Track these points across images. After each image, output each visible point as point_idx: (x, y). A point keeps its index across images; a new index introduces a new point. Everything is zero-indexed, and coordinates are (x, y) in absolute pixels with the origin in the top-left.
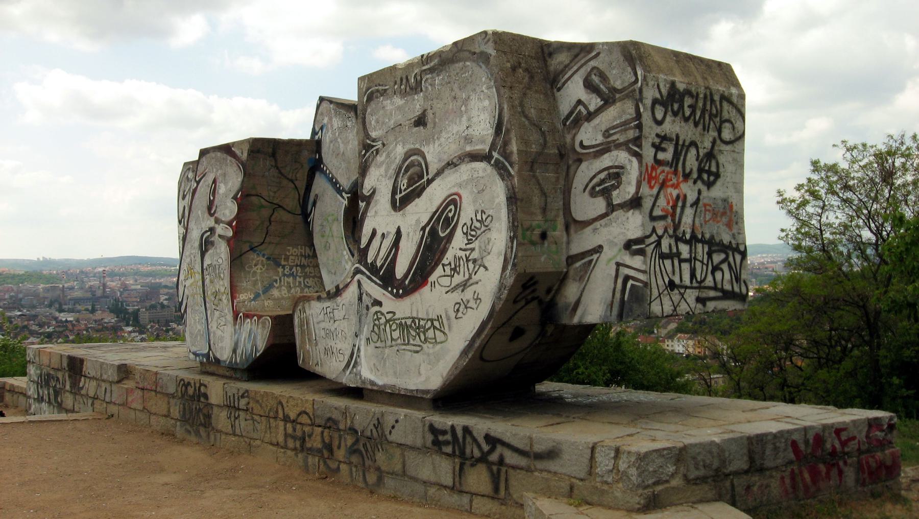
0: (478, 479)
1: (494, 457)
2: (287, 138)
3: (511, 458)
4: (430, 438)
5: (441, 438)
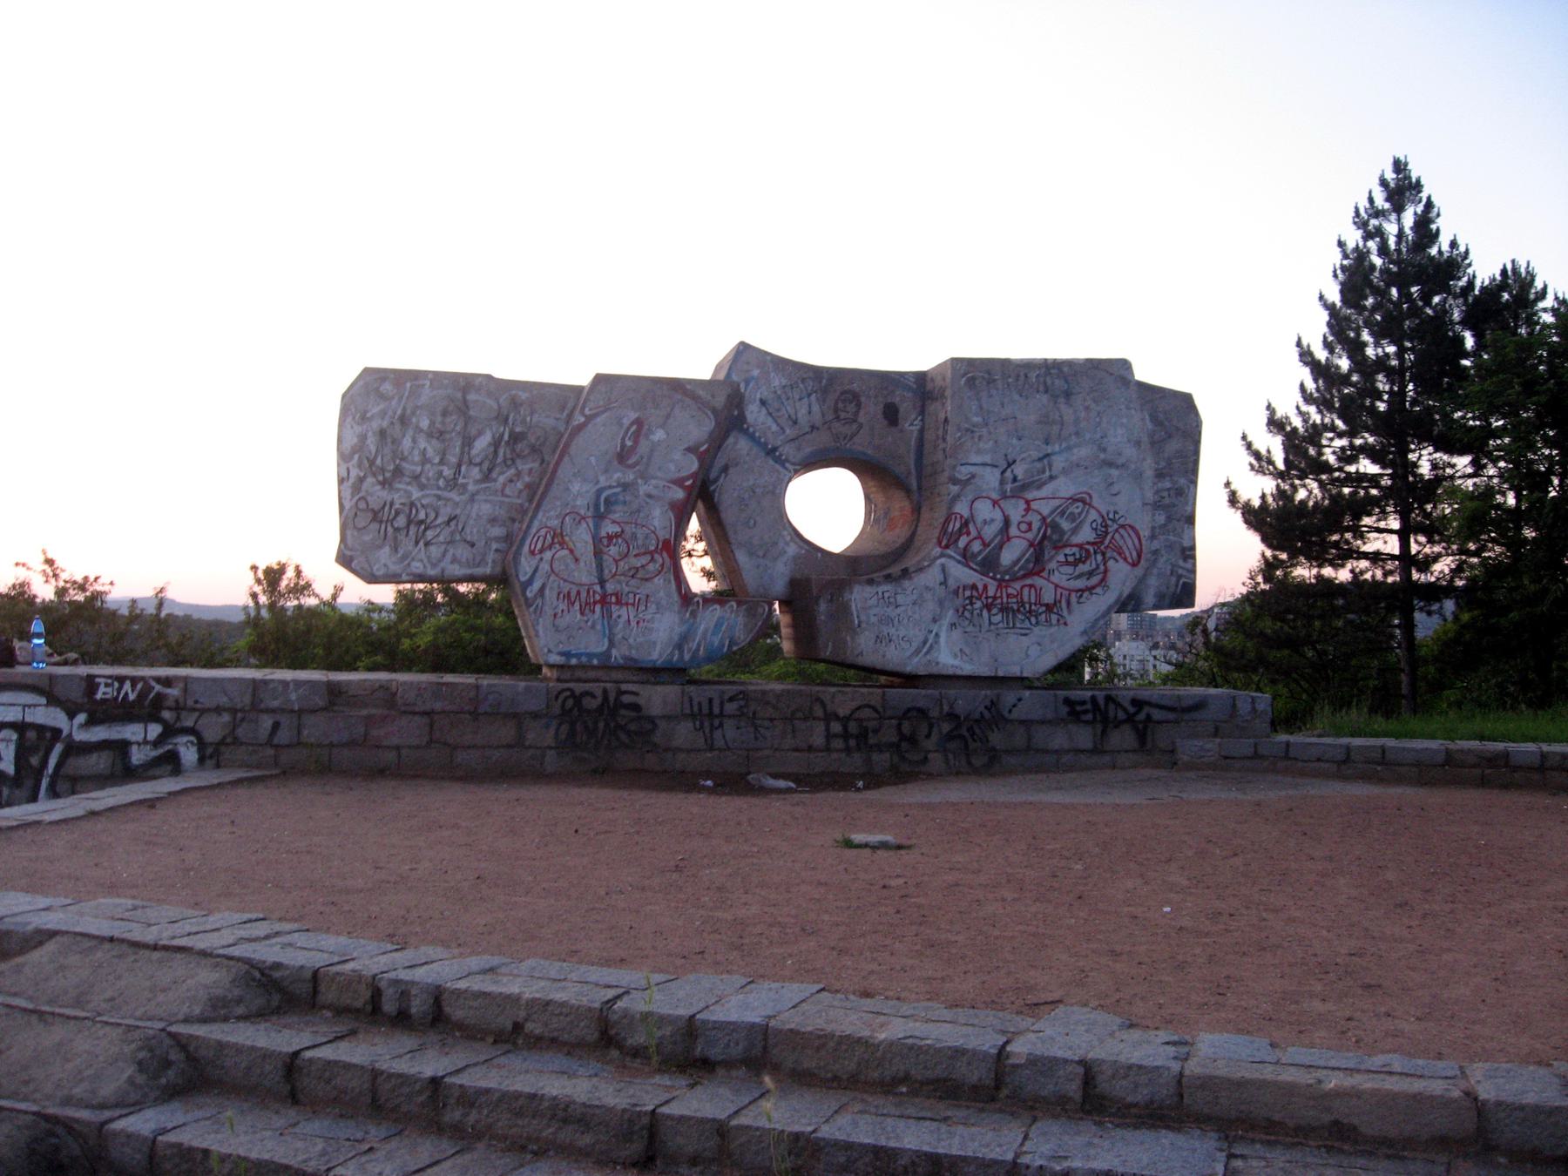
0: (1122, 738)
1: (1142, 716)
2: (573, 369)
3: (1157, 715)
4: (1064, 710)
5: (1078, 708)
